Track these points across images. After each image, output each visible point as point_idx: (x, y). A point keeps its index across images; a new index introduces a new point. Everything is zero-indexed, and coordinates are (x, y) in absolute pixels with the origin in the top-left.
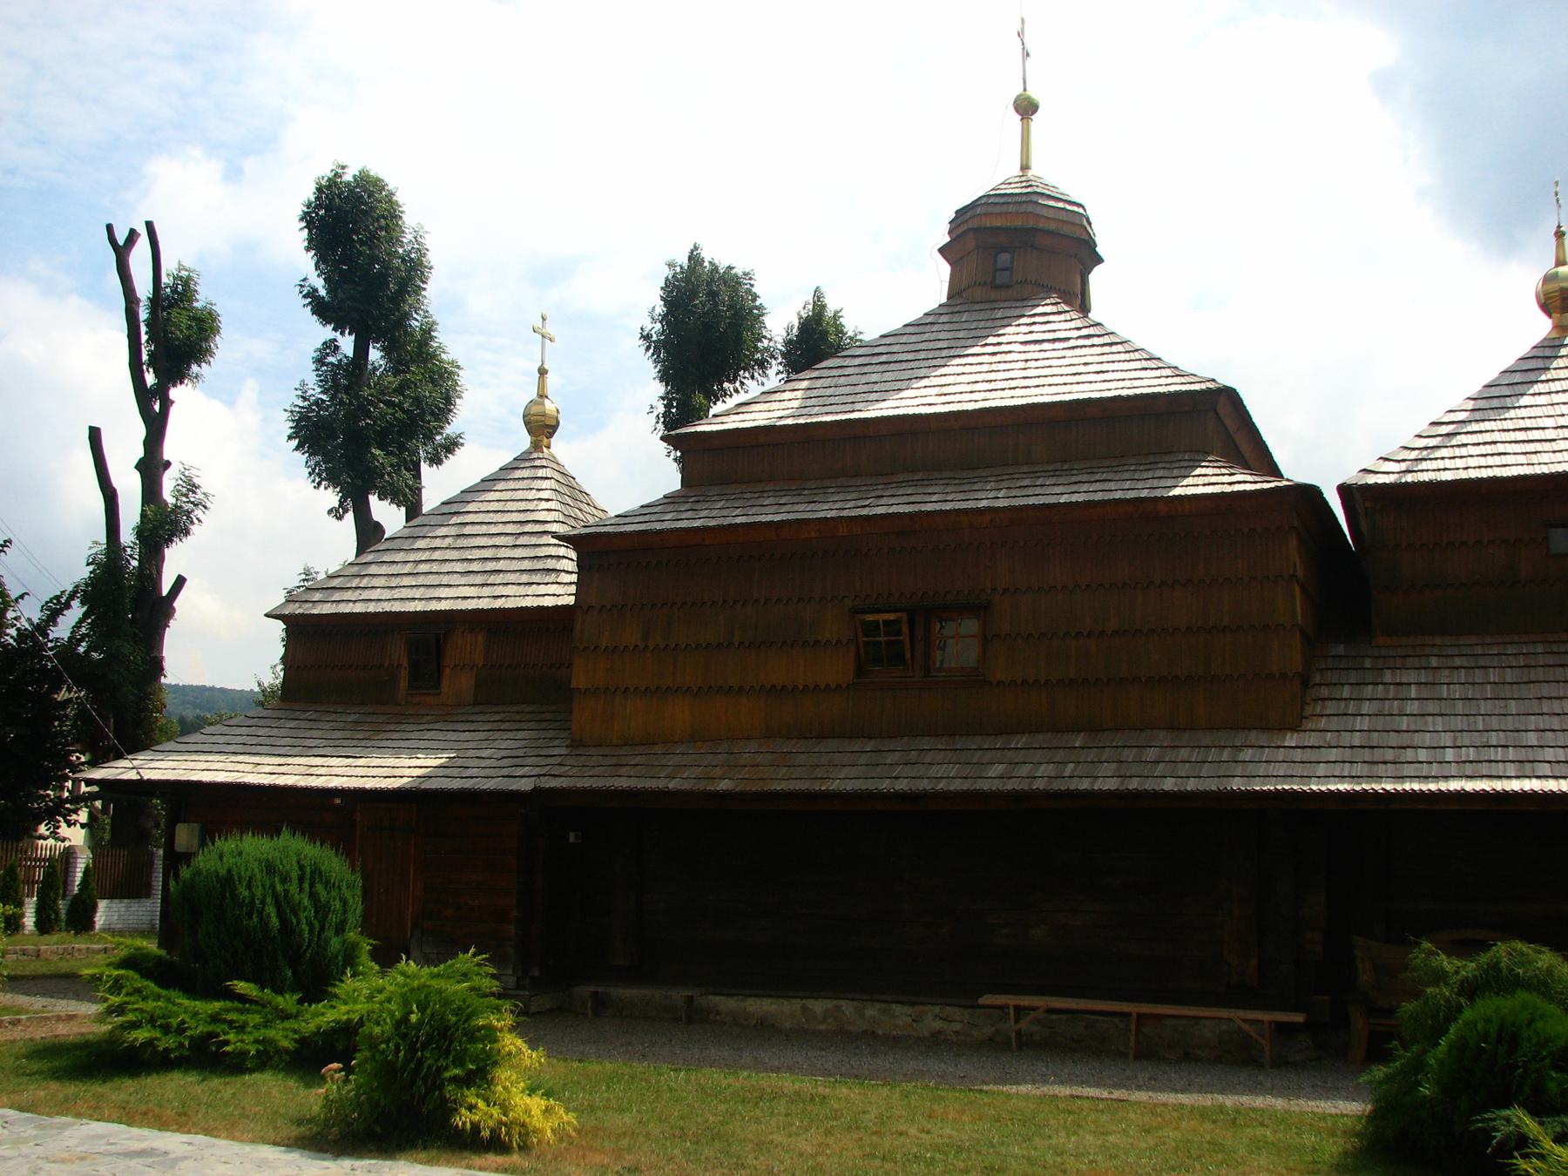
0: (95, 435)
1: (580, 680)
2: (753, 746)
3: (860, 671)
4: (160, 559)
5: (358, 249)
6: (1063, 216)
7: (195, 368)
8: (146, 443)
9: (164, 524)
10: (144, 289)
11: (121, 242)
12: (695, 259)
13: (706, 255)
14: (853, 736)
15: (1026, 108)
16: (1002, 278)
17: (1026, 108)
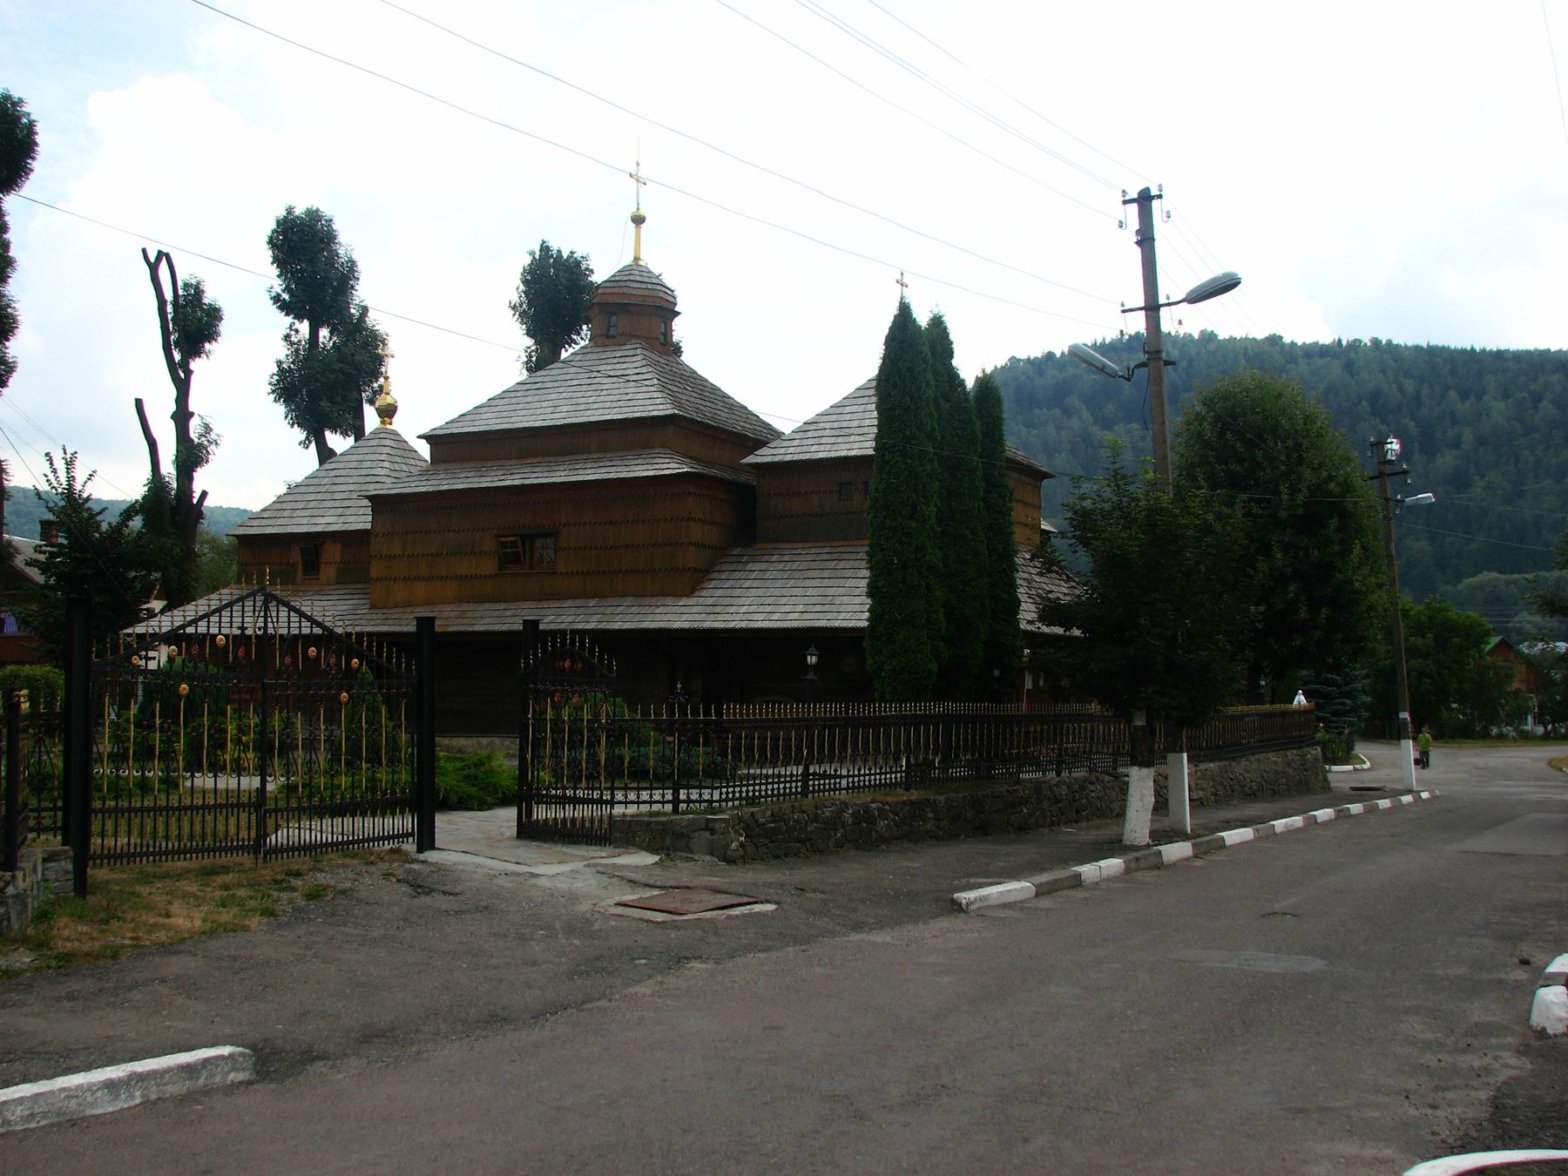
0: (139, 404)
1: (374, 573)
2: (451, 607)
3: (502, 566)
4: (191, 479)
5: (309, 261)
6: (647, 293)
7: (207, 346)
8: (177, 401)
9: (191, 456)
10: (169, 296)
11: (152, 259)
12: (545, 248)
13: (554, 246)
14: (498, 601)
15: (638, 220)
16: (613, 331)
17: (638, 220)
